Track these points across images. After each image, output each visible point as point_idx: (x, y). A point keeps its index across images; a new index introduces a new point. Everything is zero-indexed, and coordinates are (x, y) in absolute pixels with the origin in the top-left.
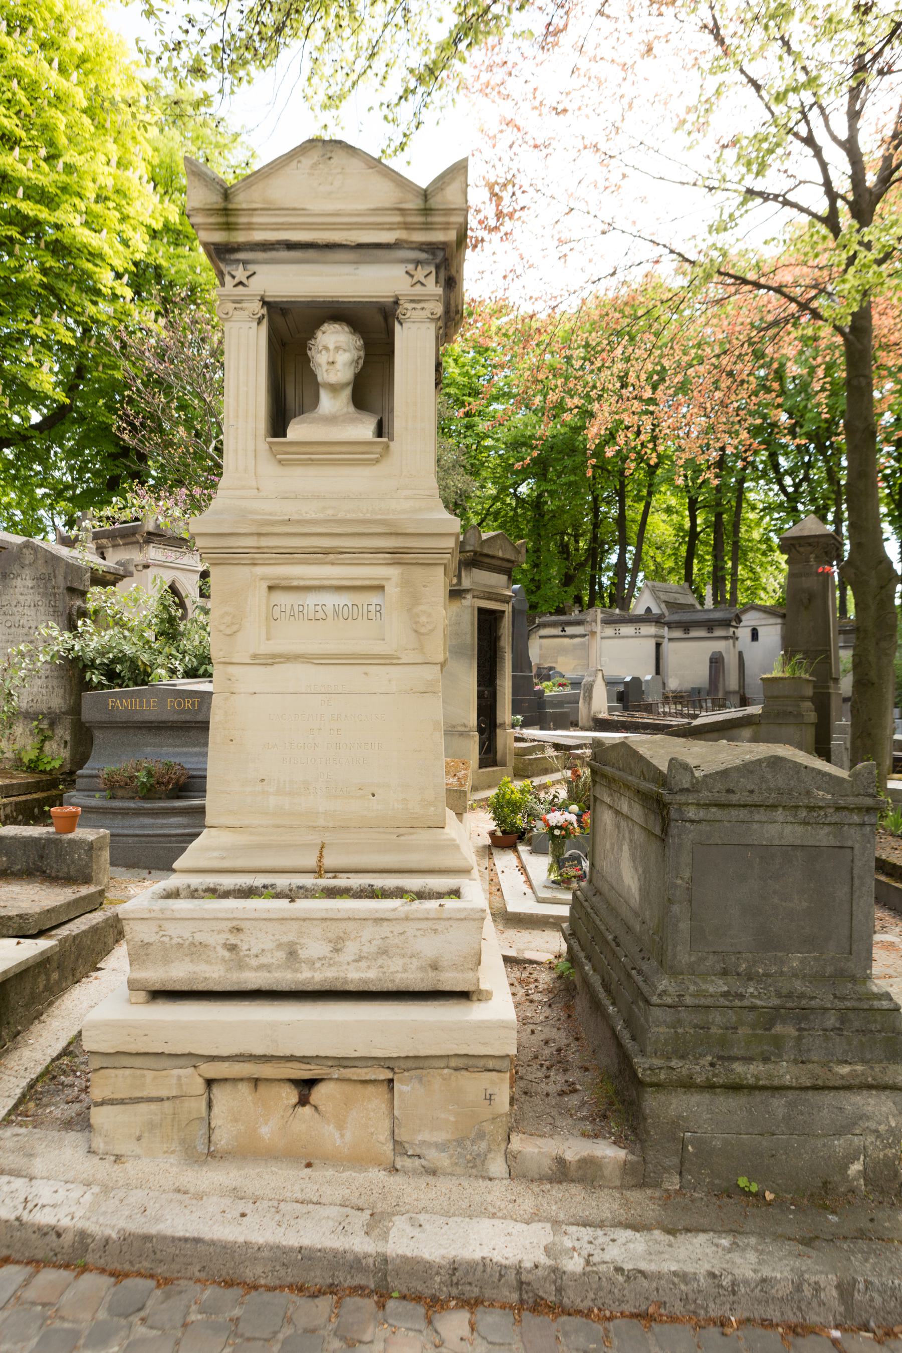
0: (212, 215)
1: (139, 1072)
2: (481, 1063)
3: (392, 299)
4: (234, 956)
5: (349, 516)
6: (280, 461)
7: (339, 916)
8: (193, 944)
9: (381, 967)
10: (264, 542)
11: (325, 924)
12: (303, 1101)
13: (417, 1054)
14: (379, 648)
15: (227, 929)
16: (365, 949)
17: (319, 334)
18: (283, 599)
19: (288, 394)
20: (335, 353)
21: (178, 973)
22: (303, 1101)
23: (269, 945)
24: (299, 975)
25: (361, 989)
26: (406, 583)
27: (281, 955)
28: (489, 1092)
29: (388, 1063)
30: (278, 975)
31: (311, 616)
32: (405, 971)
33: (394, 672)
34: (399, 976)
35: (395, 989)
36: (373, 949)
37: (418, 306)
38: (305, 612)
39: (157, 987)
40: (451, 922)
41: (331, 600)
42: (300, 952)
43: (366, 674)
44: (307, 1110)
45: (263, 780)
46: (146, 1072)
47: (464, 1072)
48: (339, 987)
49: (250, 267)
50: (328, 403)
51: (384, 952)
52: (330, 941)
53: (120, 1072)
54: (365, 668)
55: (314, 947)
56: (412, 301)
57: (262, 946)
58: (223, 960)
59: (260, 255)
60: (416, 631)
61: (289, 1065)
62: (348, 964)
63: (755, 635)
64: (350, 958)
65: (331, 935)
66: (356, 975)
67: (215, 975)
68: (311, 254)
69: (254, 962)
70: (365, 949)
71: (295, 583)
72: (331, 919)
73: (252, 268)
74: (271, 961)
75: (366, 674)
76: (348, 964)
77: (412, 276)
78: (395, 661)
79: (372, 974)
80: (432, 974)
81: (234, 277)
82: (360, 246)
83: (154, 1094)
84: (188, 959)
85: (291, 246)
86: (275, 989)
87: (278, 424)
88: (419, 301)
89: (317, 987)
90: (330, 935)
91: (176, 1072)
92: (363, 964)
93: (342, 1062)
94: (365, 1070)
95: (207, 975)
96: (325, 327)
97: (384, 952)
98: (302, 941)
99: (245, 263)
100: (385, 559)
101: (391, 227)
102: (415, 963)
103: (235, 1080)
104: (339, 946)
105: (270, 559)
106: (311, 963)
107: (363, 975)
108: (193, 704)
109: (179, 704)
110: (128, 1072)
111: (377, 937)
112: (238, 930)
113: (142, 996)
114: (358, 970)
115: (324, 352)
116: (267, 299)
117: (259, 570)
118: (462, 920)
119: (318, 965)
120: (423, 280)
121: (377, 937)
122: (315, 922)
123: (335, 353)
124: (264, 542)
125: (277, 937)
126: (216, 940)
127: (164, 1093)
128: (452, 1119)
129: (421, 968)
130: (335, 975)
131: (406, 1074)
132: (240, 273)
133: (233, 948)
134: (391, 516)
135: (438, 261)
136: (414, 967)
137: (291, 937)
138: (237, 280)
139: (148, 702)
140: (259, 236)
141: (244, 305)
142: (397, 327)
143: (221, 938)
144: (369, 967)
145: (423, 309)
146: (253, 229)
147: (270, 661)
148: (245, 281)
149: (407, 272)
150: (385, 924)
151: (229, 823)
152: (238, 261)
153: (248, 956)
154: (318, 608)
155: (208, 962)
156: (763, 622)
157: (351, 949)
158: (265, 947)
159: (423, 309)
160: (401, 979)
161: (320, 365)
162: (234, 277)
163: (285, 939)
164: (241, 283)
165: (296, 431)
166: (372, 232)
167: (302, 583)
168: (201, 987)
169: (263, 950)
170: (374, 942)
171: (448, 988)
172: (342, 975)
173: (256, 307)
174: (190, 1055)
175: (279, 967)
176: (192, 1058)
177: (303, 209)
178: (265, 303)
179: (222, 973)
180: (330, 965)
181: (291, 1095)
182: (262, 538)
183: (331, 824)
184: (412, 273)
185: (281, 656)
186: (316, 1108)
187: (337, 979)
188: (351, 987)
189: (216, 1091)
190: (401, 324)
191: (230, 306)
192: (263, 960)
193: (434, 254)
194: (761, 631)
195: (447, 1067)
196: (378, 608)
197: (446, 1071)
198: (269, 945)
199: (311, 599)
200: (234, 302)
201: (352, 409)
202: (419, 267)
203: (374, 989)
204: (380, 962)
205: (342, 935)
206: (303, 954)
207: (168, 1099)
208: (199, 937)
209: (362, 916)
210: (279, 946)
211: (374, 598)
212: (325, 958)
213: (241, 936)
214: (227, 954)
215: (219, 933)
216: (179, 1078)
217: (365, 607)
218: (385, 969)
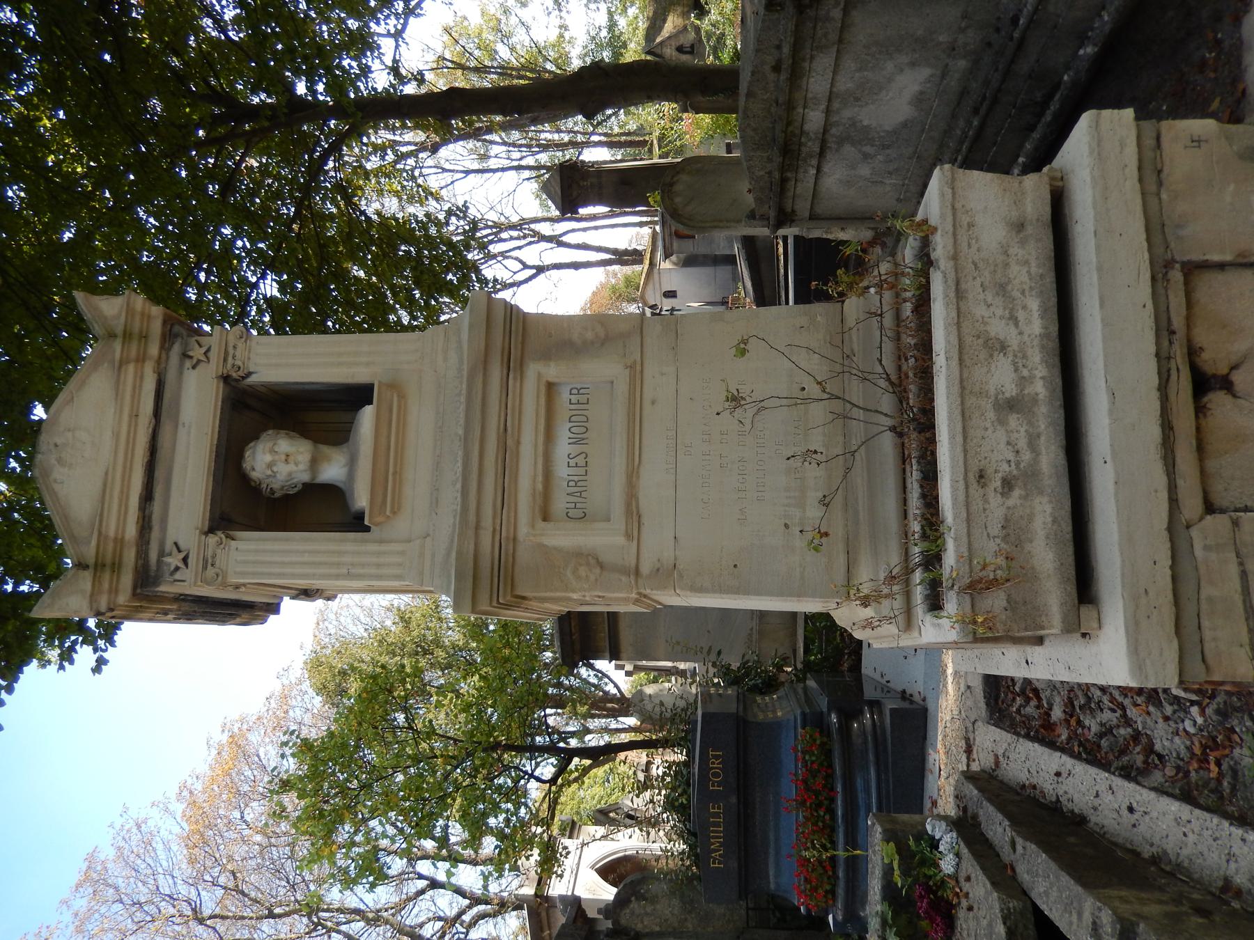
0: (100, 582)
1: (1204, 606)
2: (1149, 154)
3: (221, 385)
4: (1020, 483)
5: (462, 422)
6: (394, 513)
7: (956, 342)
8: (1005, 538)
9: (1023, 293)
10: (487, 522)
11: (968, 362)
12: (1226, 384)
13: (1143, 229)
14: (622, 388)
15: (981, 491)
16: (999, 312)
17: (255, 475)
18: (561, 502)
19: (319, 508)
20: (279, 460)
21: (1047, 558)
22: (1226, 384)
23: (1001, 435)
24: (1041, 397)
25: (1055, 317)
26: (547, 355)
27: (1013, 420)
28: (1190, 144)
29: (1160, 270)
30: (1042, 425)
31: (582, 471)
32: (1027, 262)
33: (651, 369)
34: (1034, 270)
35: (1053, 274)
36: (999, 301)
37: (231, 351)
38: (576, 478)
39: (1072, 589)
40: (958, 206)
41: (563, 448)
42: (1008, 395)
43: (653, 403)
44: (1237, 377)
45: (786, 526)
46: (1203, 596)
47: (1163, 175)
48: (1054, 344)
49: (167, 550)
50: (333, 471)
51: (1002, 288)
52: (991, 356)
53: (1207, 635)
54: (647, 404)
55: (1000, 446)
56: (225, 360)
57: (1002, 446)
58: (1025, 497)
59: (155, 535)
60: (603, 344)
61: (1172, 397)
62: (1021, 333)
63: (671, 294)
64: (1013, 331)
65: (983, 355)
66: (1035, 322)
67: (1048, 509)
68: (159, 474)
69: (1027, 456)
70: (999, 312)
71: (540, 487)
72: (960, 353)
73: (169, 545)
74: (1023, 433)
75: (653, 403)
76: (1021, 333)
77: (199, 361)
78: (638, 368)
79: (1034, 305)
80: (1029, 230)
81: (177, 569)
82: (157, 413)
83: (1236, 584)
84: (1028, 547)
85: (147, 496)
86: (1063, 428)
87: (356, 523)
88: (226, 353)
89: (1061, 413)
90: (982, 357)
91: (1199, 552)
92: (1021, 315)
93: (1164, 329)
94: (1171, 297)
95: (1049, 519)
96: (247, 465)
97: (1002, 288)
98: (992, 392)
99: (162, 554)
100: (515, 379)
101: (140, 377)
102: (1015, 250)
103: (1203, 473)
104: (998, 346)
105: (508, 517)
106: (1022, 382)
107: (1036, 314)
108: (716, 757)
109: (716, 775)
110: (1206, 623)
111: (982, 296)
112: (981, 477)
113: (1086, 611)
114: (1029, 322)
115: (275, 469)
116: (206, 529)
117: (523, 530)
118: (954, 194)
119: (1025, 373)
120: (203, 350)
121: (982, 296)
122: (965, 375)
123: (279, 460)
124: (487, 522)
125: (988, 425)
126: (996, 507)
127: (1233, 570)
128: (1232, 187)
129: (1023, 243)
130: (1037, 350)
131: (1172, 245)
132: (174, 561)
133: (1008, 484)
134: (465, 373)
135: (185, 333)
136: (1021, 252)
137: (988, 405)
138: (181, 565)
139: (717, 815)
140: (131, 531)
141: (210, 553)
142: (253, 379)
143: (995, 501)
144: (1024, 307)
145: (235, 347)
146: (123, 538)
147: (636, 518)
148: (182, 555)
149: (194, 367)
150: (963, 286)
151: (843, 569)
152: (159, 562)
153: (1018, 464)
154: (572, 463)
155: (1031, 518)
156: (657, 286)
157: (999, 328)
158: (1004, 439)
159: (235, 347)
160: (1038, 266)
161: (290, 474)
162: (177, 569)
163: (991, 415)
164: (185, 560)
165: (361, 500)
166: (142, 400)
167: (540, 478)
168: (1067, 527)
169: (1008, 443)
170: (990, 299)
171: (1048, 209)
172: (1036, 342)
173: (212, 540)
174: (1171, 529)
175: (1030, 423)
176: (1176, 529)
177: (106, 474)
178: (211, 530)
179: (1045, 499)
180: (1025, 357)
181: (1218, 400)
182: (483, 524)
183: (841, 439)
184: (195, 361)
185: (628, 505)
186: (1234, 368)
187: (1043, 347)
188: (1054, 329)
189: (1220, 500)
190: (249, 374)
191: (211, 572)
192: (1022, 443)
193: (176, 336)
194: (667, 287)
195: (1158, 194)
196: (575, 391)
197: (1164, 196)
198: (1001, 435)
199: (562, 471)
200: (205, 568)
201: (344, 448)
202: (191, 353)
203: (1054, 300)
204: (1016, 294)
205: (981, 341)
206: (1010, 390)
207: (1241, 564)
208: (995, 530)
209: (954, 314)
210: (1002, 422)
211: (564, 395)
212: (1014, 364)
213: (990, 471)
214: (1017, 493)
215: (986, 502)
216: (1207, 548)
217: (573, 407)
218: (1026, 287)
